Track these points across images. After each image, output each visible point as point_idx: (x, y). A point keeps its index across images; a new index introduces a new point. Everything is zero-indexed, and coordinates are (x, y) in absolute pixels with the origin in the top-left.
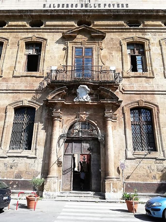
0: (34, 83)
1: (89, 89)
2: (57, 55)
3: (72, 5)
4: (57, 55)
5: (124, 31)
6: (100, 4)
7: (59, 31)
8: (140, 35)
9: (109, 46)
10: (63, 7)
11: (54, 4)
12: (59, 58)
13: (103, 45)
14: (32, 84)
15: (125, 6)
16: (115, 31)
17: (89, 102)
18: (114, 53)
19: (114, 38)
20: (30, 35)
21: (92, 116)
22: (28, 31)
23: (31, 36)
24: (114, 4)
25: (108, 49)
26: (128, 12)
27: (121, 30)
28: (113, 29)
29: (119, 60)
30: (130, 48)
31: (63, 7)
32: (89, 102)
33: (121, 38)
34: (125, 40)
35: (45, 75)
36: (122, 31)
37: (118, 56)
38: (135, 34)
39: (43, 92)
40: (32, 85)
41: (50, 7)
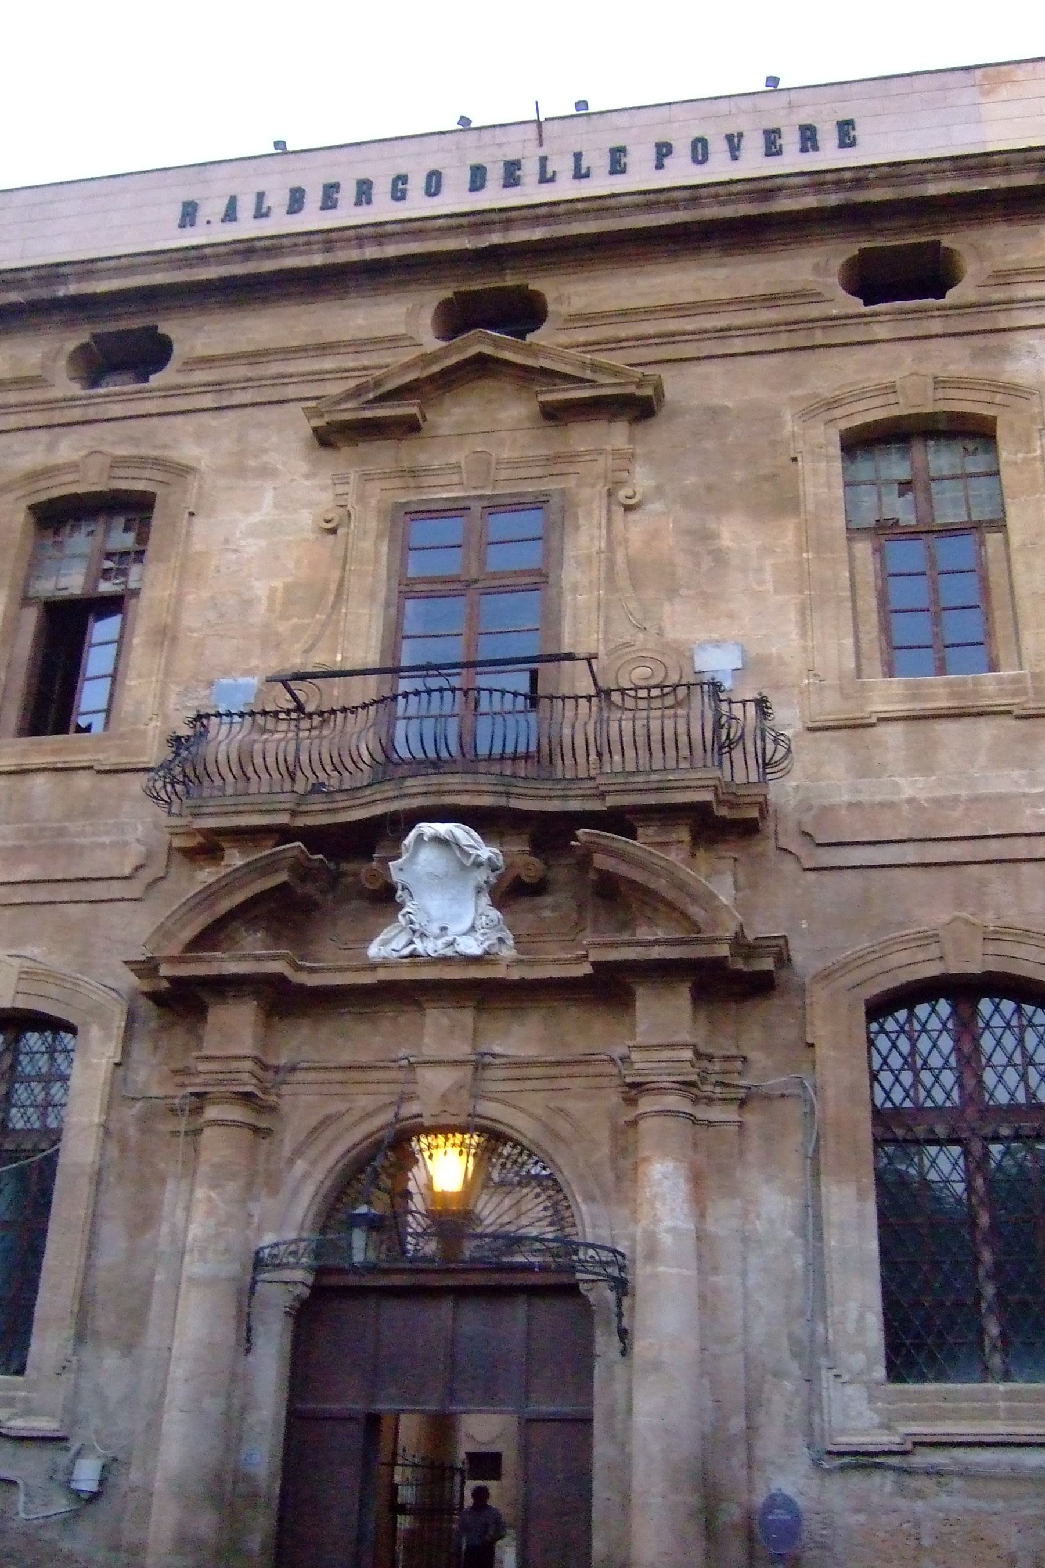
0: (72, 827)
1: (486, 852)
2: (260, 588)
3: (402, 179)
4: (260, 588)
5: (819, 337)
6: (622, 150)
7: (291, 392)
8: (954, 359)
9: (691, 480)
10: (399, 194)
11: (261, 196)
12: (278, 607)
13: (642, 480)
14: (61, 832)
15: (828, 137)
16: (738, 345)
17: (494, 963)
18: (733, 532)
19: (730, 404)
20: (68, 449)
21: (529, 1085)
22: (58, 417)
23: (76, 456)
24: (740, 135)
25: (688, 501)
26: (672, 205)
27: (802, 336)
28: (723, 333)
29: (770, 587)
30: (877, 471)
31: (399, 194)
32: (494, 963)
33: (792, 398)
34: (828, 416)
35: (154, 753)
36: (799, 339)
37: (766, 550)
38: (908, 361)
39: (137, 895)
40: (61, 840)
41: (230, 215)
